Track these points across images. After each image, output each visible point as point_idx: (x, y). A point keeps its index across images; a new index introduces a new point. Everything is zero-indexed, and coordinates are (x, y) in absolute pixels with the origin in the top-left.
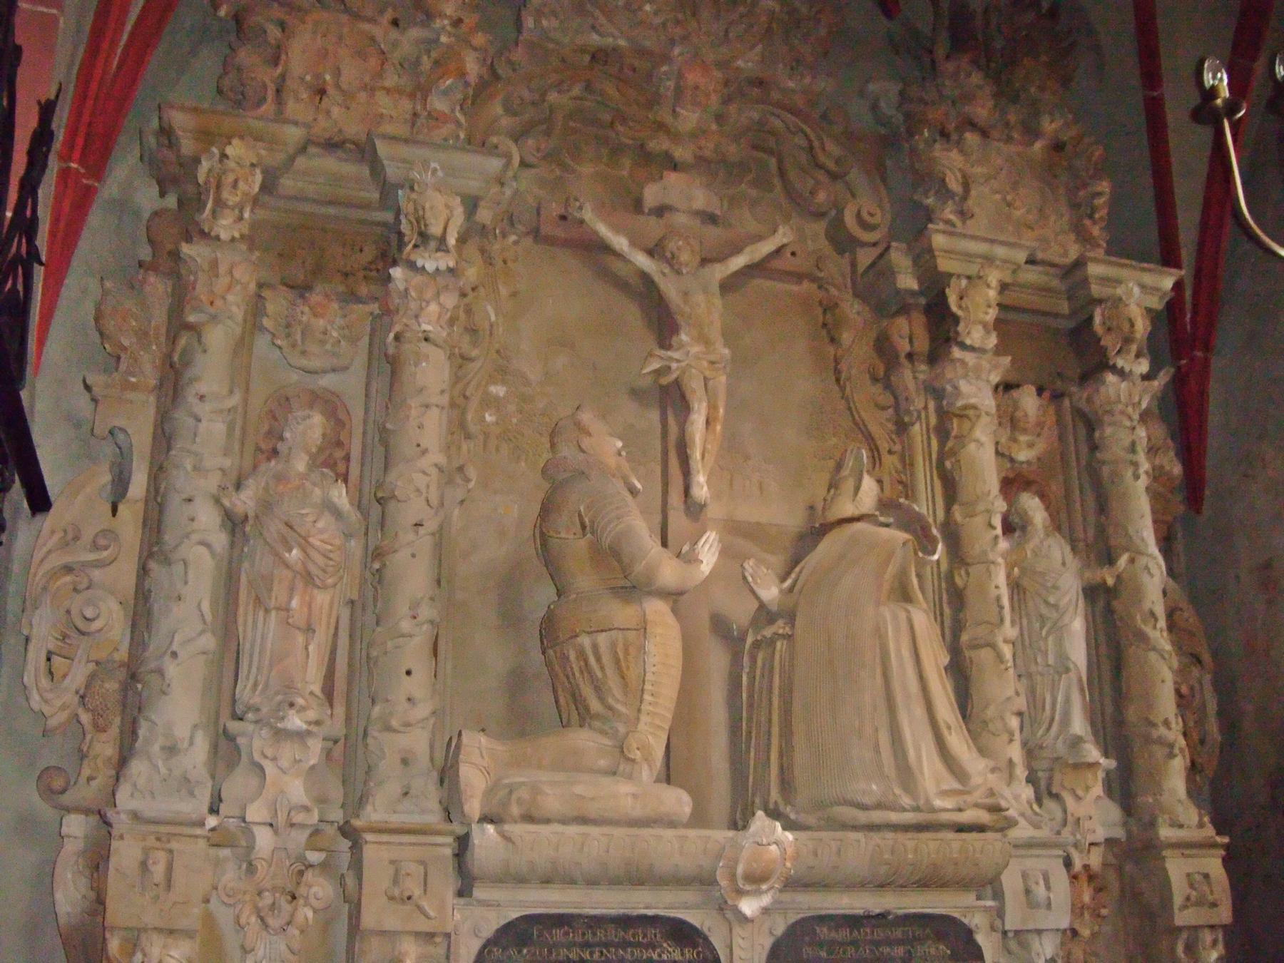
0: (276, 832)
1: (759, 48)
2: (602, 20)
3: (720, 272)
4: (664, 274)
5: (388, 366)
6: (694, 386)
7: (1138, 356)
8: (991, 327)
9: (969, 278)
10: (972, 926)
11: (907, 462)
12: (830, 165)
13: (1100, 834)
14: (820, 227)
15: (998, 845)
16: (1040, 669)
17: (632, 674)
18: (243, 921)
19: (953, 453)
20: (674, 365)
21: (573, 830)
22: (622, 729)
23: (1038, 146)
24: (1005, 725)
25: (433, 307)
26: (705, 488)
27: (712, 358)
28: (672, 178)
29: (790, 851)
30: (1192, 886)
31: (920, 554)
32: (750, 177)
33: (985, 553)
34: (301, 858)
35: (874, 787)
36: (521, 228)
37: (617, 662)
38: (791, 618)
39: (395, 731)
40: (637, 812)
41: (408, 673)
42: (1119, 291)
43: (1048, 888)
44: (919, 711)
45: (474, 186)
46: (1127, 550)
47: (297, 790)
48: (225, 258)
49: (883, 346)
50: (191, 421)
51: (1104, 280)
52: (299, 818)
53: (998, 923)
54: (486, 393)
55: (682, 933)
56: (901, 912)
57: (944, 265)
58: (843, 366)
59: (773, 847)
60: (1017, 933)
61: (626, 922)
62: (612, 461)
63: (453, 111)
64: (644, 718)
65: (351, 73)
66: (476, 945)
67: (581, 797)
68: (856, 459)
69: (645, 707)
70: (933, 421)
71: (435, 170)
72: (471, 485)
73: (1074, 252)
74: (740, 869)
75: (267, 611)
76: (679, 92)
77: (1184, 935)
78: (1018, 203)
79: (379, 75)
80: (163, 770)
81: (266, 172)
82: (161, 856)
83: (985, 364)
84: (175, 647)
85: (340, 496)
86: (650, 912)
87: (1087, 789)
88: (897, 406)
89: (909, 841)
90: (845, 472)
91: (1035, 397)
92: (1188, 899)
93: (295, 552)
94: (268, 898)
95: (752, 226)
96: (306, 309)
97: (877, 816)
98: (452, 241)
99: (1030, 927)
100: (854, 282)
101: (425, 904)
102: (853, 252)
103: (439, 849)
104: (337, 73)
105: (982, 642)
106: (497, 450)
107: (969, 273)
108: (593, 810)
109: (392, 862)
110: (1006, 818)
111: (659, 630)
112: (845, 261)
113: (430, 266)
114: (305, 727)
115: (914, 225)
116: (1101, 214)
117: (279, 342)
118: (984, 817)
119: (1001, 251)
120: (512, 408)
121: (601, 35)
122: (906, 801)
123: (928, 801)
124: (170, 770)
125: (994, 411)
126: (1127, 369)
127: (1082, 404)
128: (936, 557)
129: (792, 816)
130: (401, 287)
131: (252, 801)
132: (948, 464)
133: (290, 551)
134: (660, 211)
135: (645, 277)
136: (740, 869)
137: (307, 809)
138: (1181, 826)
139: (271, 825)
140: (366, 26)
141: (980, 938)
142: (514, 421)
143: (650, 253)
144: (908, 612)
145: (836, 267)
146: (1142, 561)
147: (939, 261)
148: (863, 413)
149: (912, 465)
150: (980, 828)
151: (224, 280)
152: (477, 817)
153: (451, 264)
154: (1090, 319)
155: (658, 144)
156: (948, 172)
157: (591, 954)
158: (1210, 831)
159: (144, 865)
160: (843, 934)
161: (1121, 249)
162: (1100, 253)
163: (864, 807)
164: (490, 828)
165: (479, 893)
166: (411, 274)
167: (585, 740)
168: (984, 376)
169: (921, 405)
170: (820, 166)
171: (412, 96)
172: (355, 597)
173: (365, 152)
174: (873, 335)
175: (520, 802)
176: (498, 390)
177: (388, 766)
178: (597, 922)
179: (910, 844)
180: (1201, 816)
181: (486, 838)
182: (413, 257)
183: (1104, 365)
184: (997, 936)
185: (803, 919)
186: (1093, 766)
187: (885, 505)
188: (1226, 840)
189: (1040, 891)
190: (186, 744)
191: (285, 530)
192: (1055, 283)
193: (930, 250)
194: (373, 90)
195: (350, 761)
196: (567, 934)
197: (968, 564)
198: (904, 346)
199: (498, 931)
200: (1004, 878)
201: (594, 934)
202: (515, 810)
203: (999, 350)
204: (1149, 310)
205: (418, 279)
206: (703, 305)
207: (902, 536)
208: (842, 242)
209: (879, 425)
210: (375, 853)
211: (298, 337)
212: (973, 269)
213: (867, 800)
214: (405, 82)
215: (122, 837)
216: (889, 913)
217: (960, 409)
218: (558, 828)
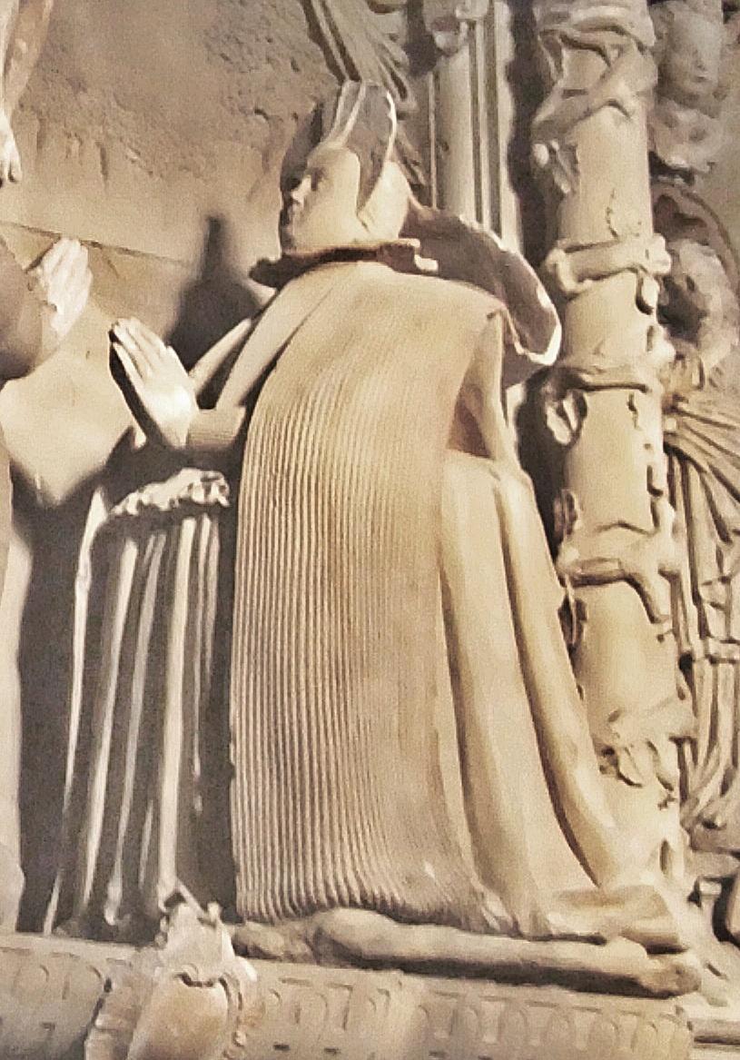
19: (559, 128)
31: (519, 349)
35: (429, 869)
70: (505, 49)
90: (334, 143)
91: (721, 23)
105: (612, 568)
132: (541, 153)
148: (337, 15)
149: (444, 145)
150: (625, 986)
179: (492, 1009)
217: (582, 27)
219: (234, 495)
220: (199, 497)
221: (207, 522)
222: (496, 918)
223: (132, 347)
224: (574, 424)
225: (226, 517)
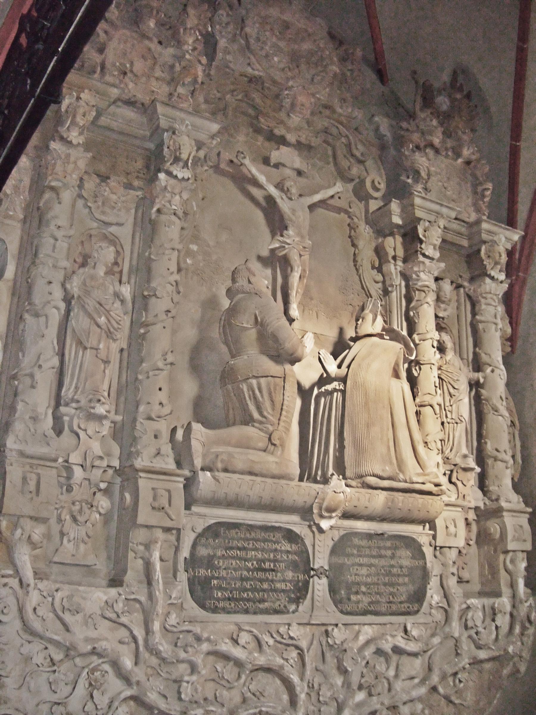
0: (84, 470)
1: (328, 90)
2: (253, 59)
4: (282, 198)
5: (148, 227)
6: (295, 258)
7: (500, 271)
8: (437, 247)
9: (430, 222)
10: (422, 543)
12: (358, 154)
13: (473, 505)
14: (350, 186)
16: (449, 420)
17: (278, 399)
18: (63, 518)
19: (415, 308)
21: (248, 478)
23: (460, 160)
26: (297, 312)
27: (304, 245)
28: (284, 149)
30: (515, 531)
34: (97, 486)
35: (387, 468)
37: (270, 394)
38: (344, 380)
39: (153, 419)
42: (495, 238)
43: (455, 527)
45: (203, 137)
46: (490, 366)
47: (96, 448)
48: (74, 153)
49: (379, 251)
50: (52, 241)
51: (489, 232)
52: (97, 463)
53: (433, 542)
54: (188, 248)
55: (291, 536)
56: (390, 533)
57: (419, 213)
58: (359, 259)
60: (441, 547)
61: (266, 528)
64: (282, 423)
65: (139, 66)
66: (193, 536)
67: (253, 461)
68: (374, 304)
69: (283, 418)
71: (187, 125)
73: (473, 217)
74: (324, 506)
75: (85, 348)
76: (293, 105)
77: (511, 554)
79: (152, 68)
80: (32, 430)
81: (97, 111)
82: (34, 477)
84: (40, 362)
85: (127, 291)
86: (277, 525)
87: (469, 480)
88: (384, 282)
90: (367, 311)
92: (514, 536)
93: (103, 318)
94: (77, 507)
96: (107, 189)
99: (447, 545)
101: (170, 513)
103: (176, 484)
104: (132, 64)
105: (427, 403)
106: (192, 278)
107: (429, 220)
108: (257, 468)
109: (153, 489)
110: (441, 490)
112: (362, 205)
113: (180, 176)
114: (105, 413)
115: (398, 190)
116: (487, 199)
117: (89, 204)
118: (434, 489)
119: (444, 210)
121: (253, 69)
124: (36, 430)
125: (435, 289)
126: (496, 277)
127: (471, 293)
130: (163, 184)
131: (73, 452)
132: (411, 314)
133: (100, 317)
136: (324, 506)
137: (101, 458)
138: (510, 502)
139: (82, 466)
140: (147, 42)
141: (424, 549)
142: (201, 264)
143: (277, 186)
145: (358, 208)
146: (497, 371)
147: (416, 211)
148: (367, 284)
149: (390, 312)
150: (430, 493)
151: (71, 166)
152: (199, 468)
154: (479, 251)
155: (279, 131)
157: (248, 544)
158: (523, 505)
159: (24, 479)
160: (364, 543)
161: (493, 217)
162: (485, 218)
163: (381, 478)
165: (194, 509)
166: (169, 178)
169: (398, 283)
170: (353, 155)
171: (169, 83)
172: (125, 347)
173: (147, 109)
174: (374, 245)
175: (222, 461)
176: (194, 247)
177: (146, 439)
178: (251, 528)
179: (401, 498)
180: (519, 499)
181: (205, 477)
183: (485, 274)
184: (432, 549)
185: (347, 534)
186: (472, 469)
188: (530, 510)
189: (452, 529)
190: (43, 417)
191: (98, 306)
192: (463, 230)
193: (413, 205)
194: (149, 77)
195: (124, 435)
196: (237, 533)
198: (391, 253)
199: (204, 529)
200: (436, 521)
201: (250, 534)
202: (220, 465)
204: (507, 250)
205: (172, 181)
206: (302, 218)
210: (144, 484)
211: (100, 204)
212: (432, 218)
214: (166, 76)
215: (11, 465)
216: (385, 533)
225: (344, 392)
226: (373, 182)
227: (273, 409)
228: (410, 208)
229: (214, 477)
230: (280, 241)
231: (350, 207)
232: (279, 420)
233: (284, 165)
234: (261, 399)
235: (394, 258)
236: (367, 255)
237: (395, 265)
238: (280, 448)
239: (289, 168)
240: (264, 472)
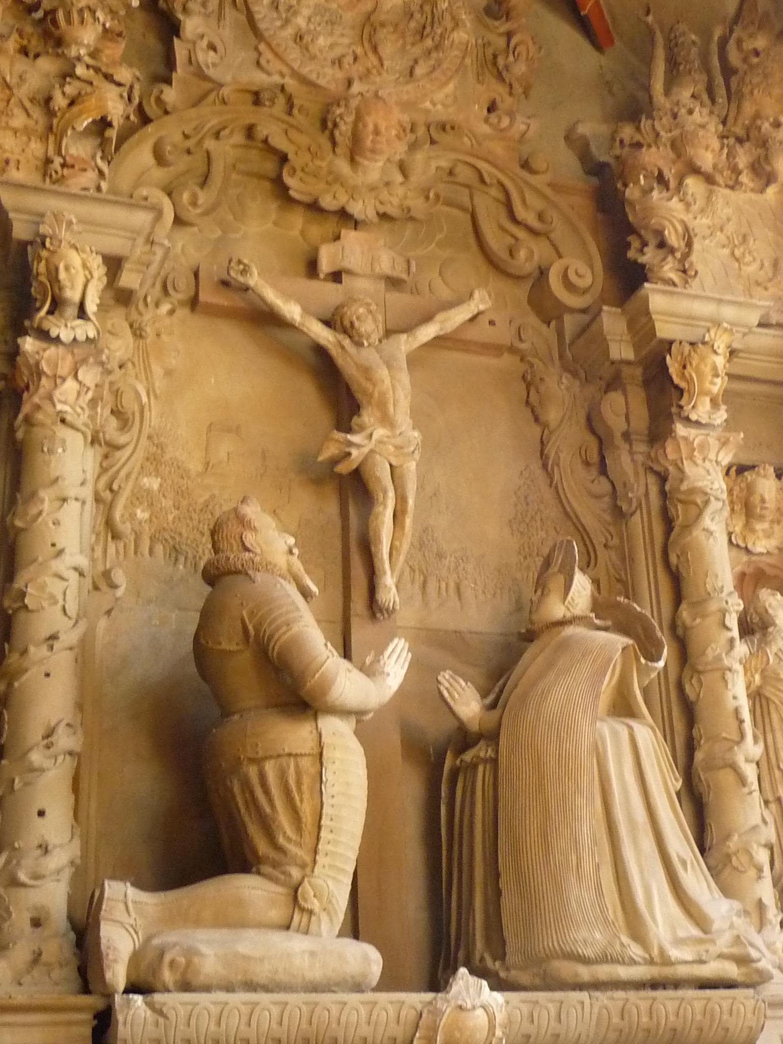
3: (404, 345)
11: (627, 558)
12: (531, 219)
14: (522, 292)
15: (750, 1004)
20: (355, 452)
21: (239, 998)
22: (295, 873)
24: (751, 857)
25: (70, 385)
28: (350, 236)
29: (500, 1018)
32: (439, 236)
33: (719, 659)
35: (598, 936)
36: (177, 297)
40: (316, 974)
41: (41, 814)
44: (648, 844)
45: (116, 245)
57: (664, 330)
58: (551, 450)
59: (480, 1012)
62: (280, 559)
63: (94, 157)
67: (247, 958)
72: (120, 592)
78: (748, 258)
83: (713, 442)
89: (639, 1000)
95: (445, 293)
97: (604, 972)
98: (91, 308)
100: (561, 356)
102: (560, 319)
108: (262, 973)
111: (337, 754)
113: (66, 335)
118: (732, 971)
119: (729, 313)
120: (167, 503)
122: (635, 951)
123: (662, 952)
128: (661, 664)
129: (502, 974)
134: (336, 277)
135: (320, 351)
143: (328, 323)
144: (630, 728)
147: (658, 325)
148: (575, 505)
149: (632, 560)
150: (730, 985)
153: (92, 334)
156: (667, 223)
164: (138, 999)
167: (251, 890)
168: (712, 456)
176: (152, 483)
182: (46, 325)
187: (596, 606)
193: (647, 313)
197: (699, 672)
202: (167, 976)
203: (729, 425)
207: (620, 641)
208: (543, 304)
209: (592, 514)
213: (589, 952)
218: (221, 996)
219: (497, 752)
220: (482, 754)
221: (488, 767)
222: (640, 957)
223: (447, 684)
224: (697, 689)
225: (495, 761)
226: (565, 276)
227: (299, 829)
228: (644, 320)
229: (150, 1005)
230: (338, 441)
231: (521, 339)
232: (316, 852)
233: (349, 272)
234: (268, 810)
235: (626, 436)
236: (570, 438)
237: (631, 453)
238: (324, 917)
239: (364, 276)
240: (282, 977)
